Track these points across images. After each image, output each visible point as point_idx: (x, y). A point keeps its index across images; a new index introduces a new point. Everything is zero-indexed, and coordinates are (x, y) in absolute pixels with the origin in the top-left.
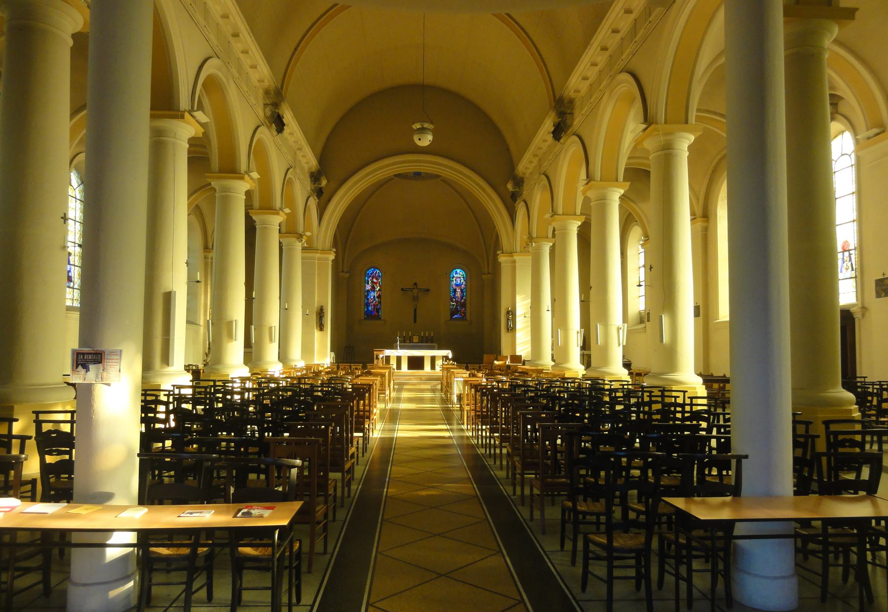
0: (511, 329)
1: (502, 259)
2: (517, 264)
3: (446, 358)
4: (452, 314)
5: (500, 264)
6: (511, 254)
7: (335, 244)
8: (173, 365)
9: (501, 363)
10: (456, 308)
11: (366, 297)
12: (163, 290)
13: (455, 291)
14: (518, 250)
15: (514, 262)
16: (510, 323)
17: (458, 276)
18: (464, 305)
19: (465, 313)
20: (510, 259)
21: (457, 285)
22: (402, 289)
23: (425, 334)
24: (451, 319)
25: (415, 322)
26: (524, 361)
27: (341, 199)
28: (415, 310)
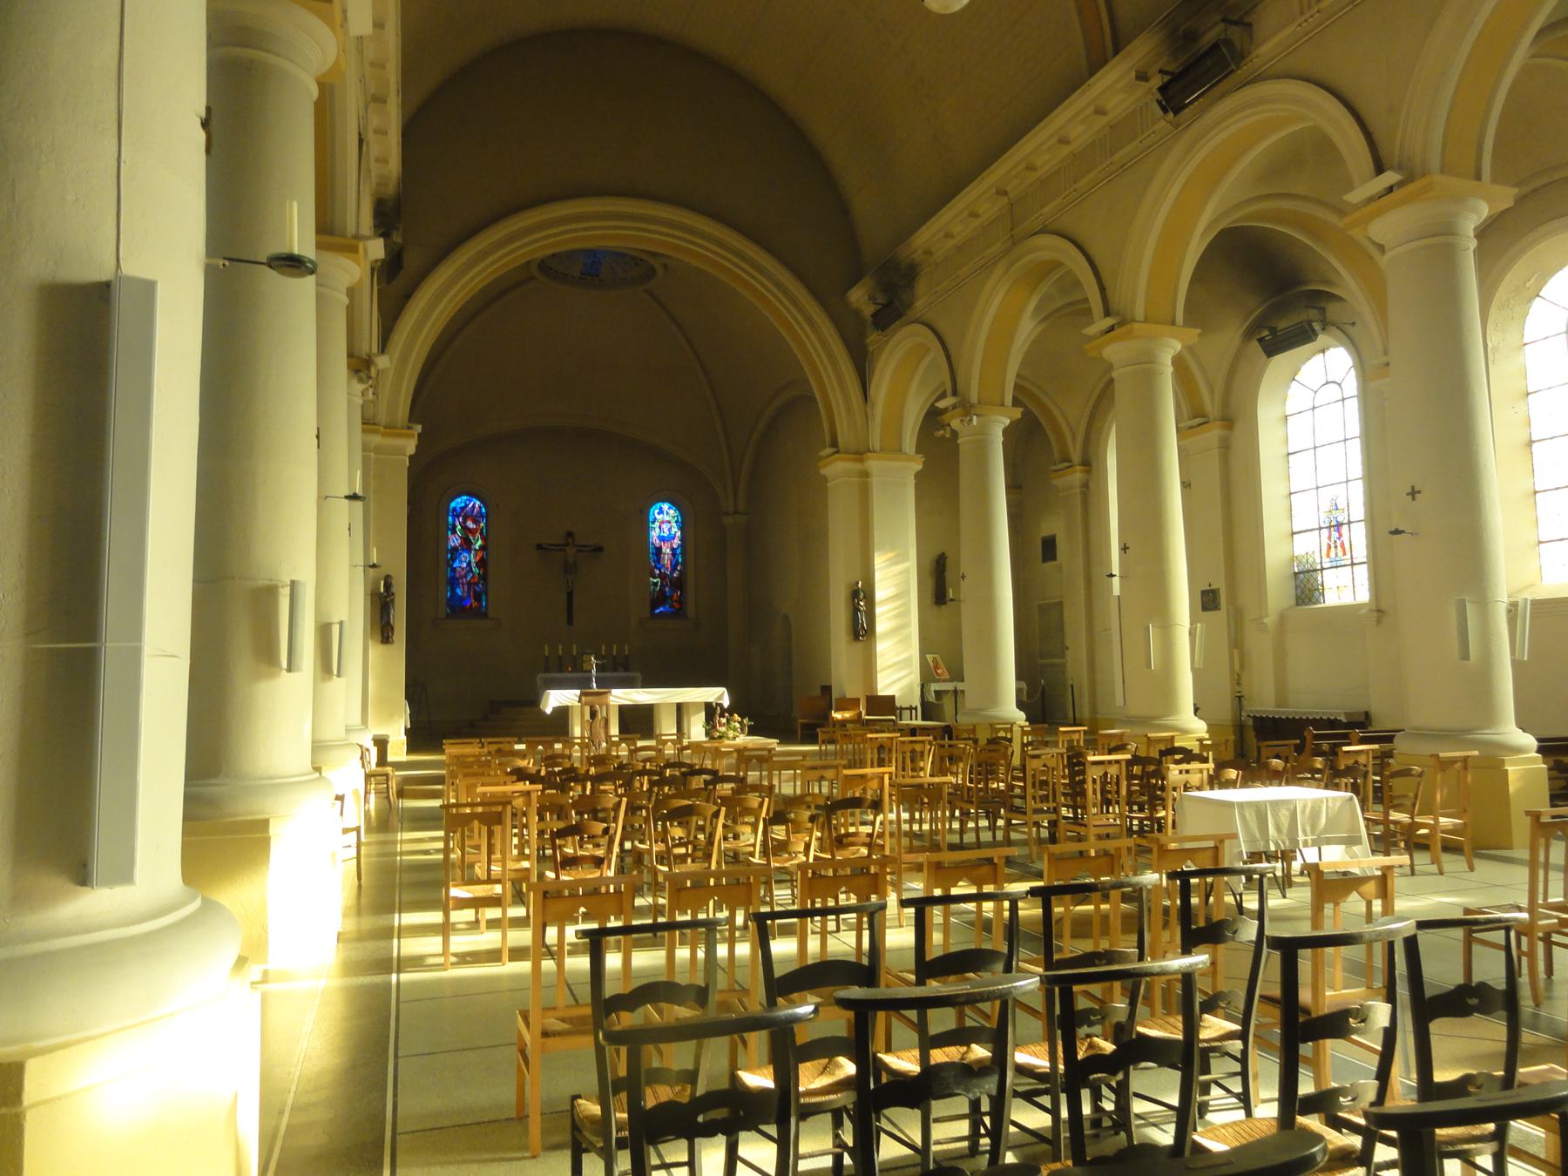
0: (862, 631)
1: (836, 469)
2: (875, 481)
3: (711, 710)
4: (655, 603)
5: (825, 479)
6: (860, 453)
7: (414, 416)
8: (124, 875)
9: (847, 715)
10: (662, 591)
11: (449, 563)
12: (36, 267)
13: (659, 550)
14: (877, 446)
15: (865, 475)
16: (862, 618)
17: (665, 522)
18: (679, 584)
19: (680, 601)
20: (857, 466)
21: (662, 539)
22: (539, 547)
23: (609, 649)
24: (653, 616)
25: (570, 621)
26: (901, 709)
27: (438, 297)
28: (570, 595)
